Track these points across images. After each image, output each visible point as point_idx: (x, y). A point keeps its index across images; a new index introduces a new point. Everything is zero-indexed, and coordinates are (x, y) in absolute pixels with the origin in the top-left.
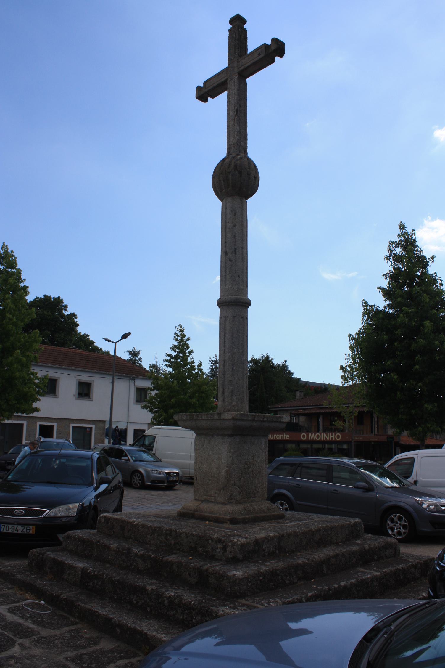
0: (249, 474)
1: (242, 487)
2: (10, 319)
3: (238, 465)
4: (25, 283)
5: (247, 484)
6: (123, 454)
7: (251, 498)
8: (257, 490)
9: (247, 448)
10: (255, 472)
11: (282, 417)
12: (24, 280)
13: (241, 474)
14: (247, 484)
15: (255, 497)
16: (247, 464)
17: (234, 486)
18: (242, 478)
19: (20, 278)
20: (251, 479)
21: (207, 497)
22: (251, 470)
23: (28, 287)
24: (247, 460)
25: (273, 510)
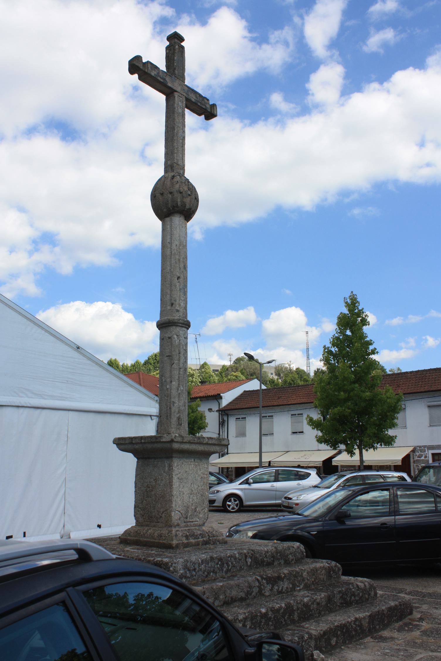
0: (151, 498)
1: (144, 510)
3: (140, 488)
5: (149, 507)
6: (337, 445)
7: (154, 523)
8: (160, 515)
10: (158, 496)
11: (162, 436)
13: (143, 497)
14: (149, 507)
15: (158, 522)
16: (149, 488)
18: (145, 501)
20: (154, 503)
21: (286, 544)
22: (153, 493)
24: (149, 484)
25: (164, 538)
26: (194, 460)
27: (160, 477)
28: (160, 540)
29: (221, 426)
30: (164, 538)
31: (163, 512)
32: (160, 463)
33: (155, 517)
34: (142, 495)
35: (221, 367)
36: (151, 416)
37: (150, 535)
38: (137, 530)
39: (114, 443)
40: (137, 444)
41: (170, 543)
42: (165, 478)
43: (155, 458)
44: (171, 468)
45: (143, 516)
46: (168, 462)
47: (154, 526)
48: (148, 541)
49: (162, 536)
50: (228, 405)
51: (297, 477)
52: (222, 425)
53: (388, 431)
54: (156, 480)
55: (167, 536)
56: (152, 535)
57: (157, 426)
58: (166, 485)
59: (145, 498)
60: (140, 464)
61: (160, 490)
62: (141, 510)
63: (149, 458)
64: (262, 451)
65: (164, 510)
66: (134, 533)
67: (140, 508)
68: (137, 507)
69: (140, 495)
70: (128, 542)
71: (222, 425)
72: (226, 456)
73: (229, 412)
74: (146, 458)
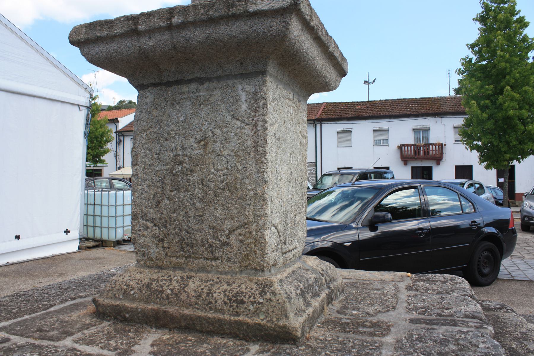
0: (187, 190)
1: (165, 226)
2: (502, 57)
4: (521, 15)
5: (181, 218)
7: (201, 260)
9: (182, 119)
10: (212, 185)
12: (520, 11)
14: (181, 218)
15: (216, 259)
17: (142, 221)
18: (166, 201)
19: (514, 10)
22: (195, 177)
23: (523, 17)
24: (180, 153)
26: (150, 38)
27: (218, 131)
28: (238, 314)
29: (118, 144)
30: (251, 308)
31: (232, 231)
32: (218, 92)
33: (203, 245)
34: (159, 184)
35: (108, 107)
36: (79, 106)
37: (200, 296)
38: (146, 281)
39: (73, 43)
40: (151, 32)
41: (285, 327)
42: (236, 134)
43: (201, 81)
44: (261, 103)
45: (162, 240)
46: (248, 88)
47: (203, 269)
48: (199, 317)
49: (243, 302)
50: (124, 128)
51: (413, 152)
52: (119, 144)
53: (307, 133)
54: (204, 142)
55: (261, 300)
56: (204, 296)
57: (85, 118)
58: (241, 153)
59: (167, 192)
60: (148, 100)
61: (220, 168)
62: (155, 225)
63: (178, 82)
64: (368, 100)
65: (237, 224)
66: (140, 290)
67: (152, 221)
68: (142, 217)
69: (149, 186)
70: (127, 315)
71: (119, 144)
72: (122, 169)
73: (125, 134)
74: (169, 84)
